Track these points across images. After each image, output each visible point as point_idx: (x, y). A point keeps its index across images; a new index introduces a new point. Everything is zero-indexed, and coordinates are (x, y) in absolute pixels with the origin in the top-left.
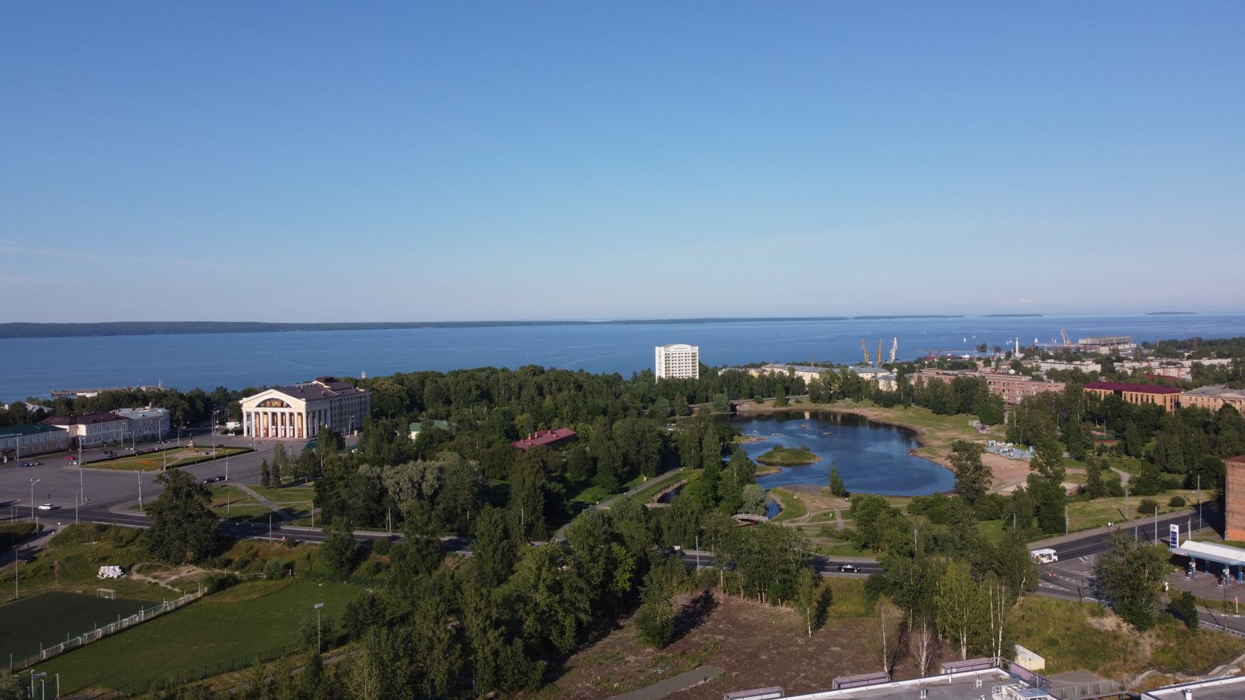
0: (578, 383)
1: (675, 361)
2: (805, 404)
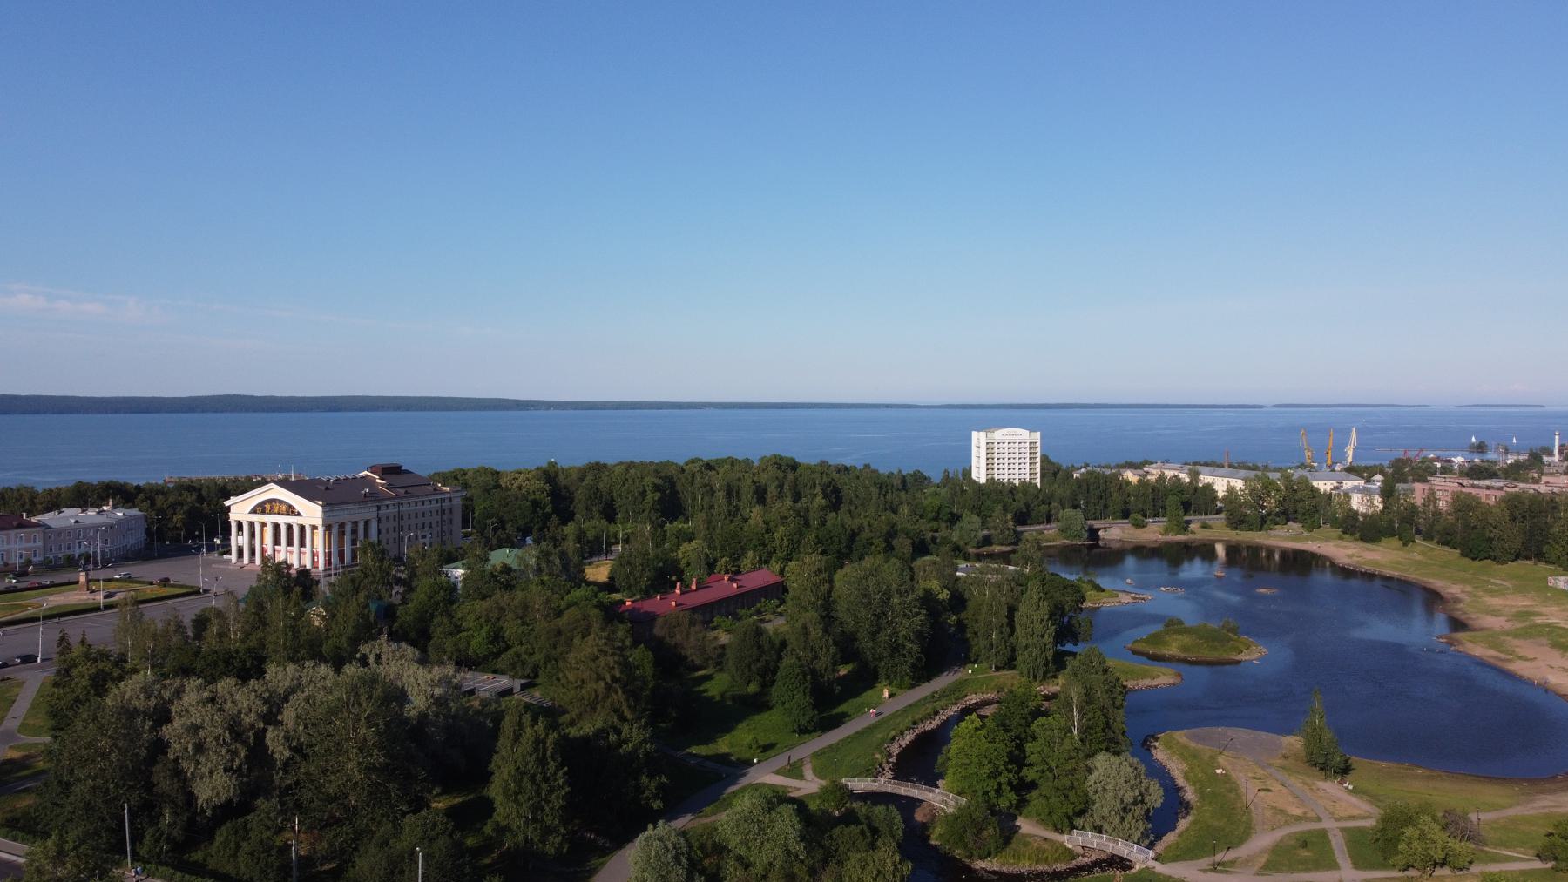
0: (836, 486)
1: (1003, 456)
2: (1219, 533)
